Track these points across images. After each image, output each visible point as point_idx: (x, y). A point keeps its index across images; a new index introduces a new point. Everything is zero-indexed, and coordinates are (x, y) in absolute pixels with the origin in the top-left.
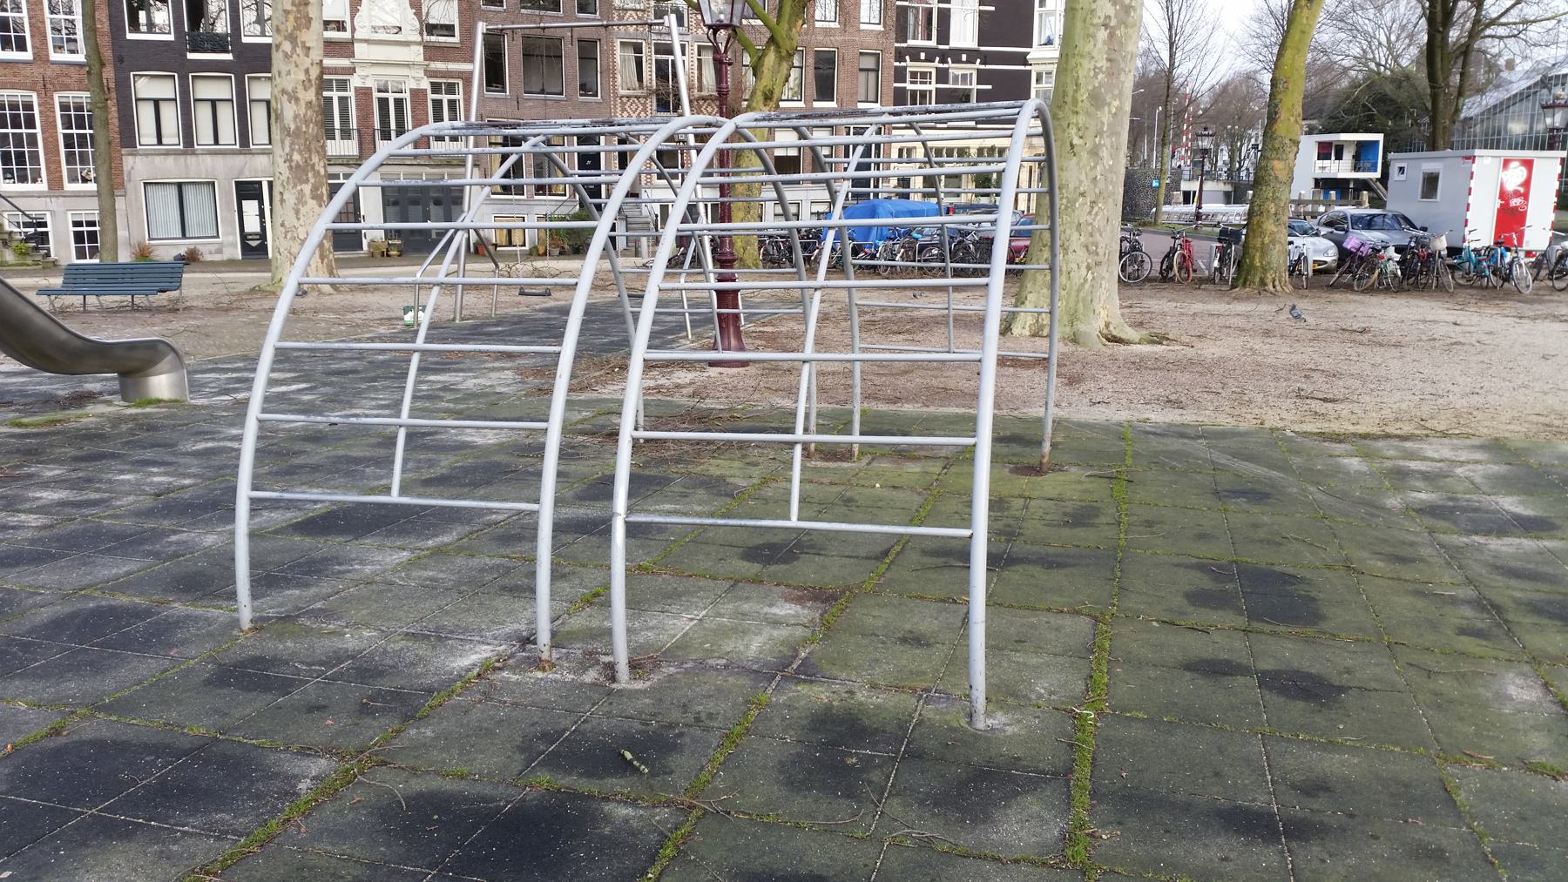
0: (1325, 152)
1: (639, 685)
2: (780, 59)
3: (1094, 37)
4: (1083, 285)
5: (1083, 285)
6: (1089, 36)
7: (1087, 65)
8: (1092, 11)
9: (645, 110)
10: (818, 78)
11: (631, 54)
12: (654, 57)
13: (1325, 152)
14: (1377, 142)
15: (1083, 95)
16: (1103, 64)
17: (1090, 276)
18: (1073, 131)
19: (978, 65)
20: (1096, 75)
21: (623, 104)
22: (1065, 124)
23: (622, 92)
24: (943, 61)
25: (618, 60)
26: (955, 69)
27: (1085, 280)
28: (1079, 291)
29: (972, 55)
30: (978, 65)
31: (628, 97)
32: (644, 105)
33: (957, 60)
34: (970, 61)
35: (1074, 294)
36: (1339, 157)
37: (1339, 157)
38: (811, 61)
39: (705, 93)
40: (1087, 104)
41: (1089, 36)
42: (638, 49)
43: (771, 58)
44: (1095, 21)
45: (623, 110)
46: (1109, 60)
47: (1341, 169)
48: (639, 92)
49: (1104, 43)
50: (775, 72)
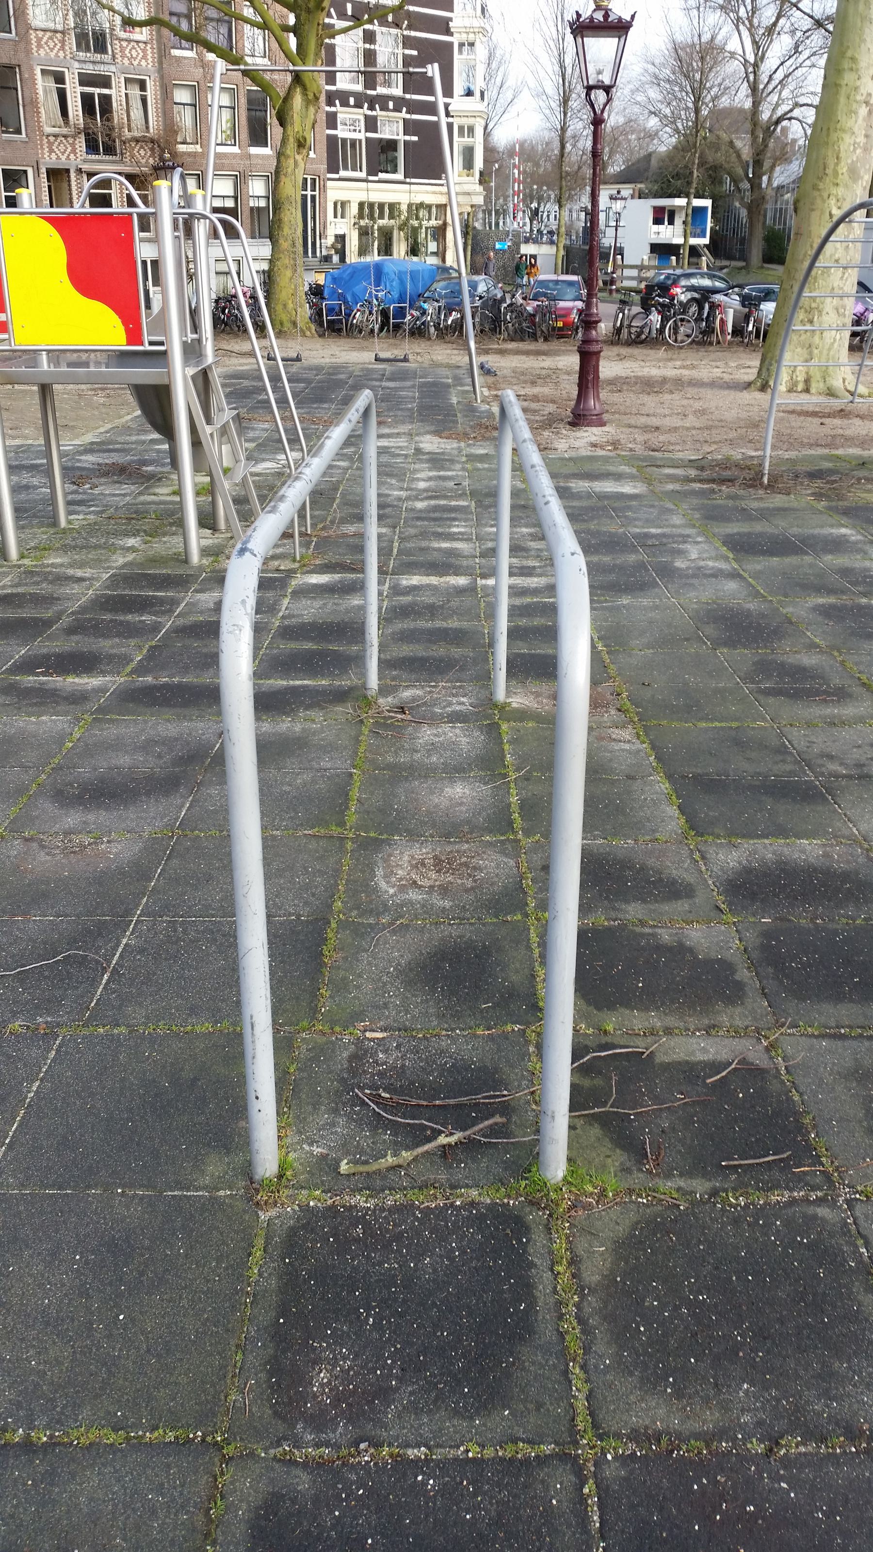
0: (660, 216)
1: (517, 701)
2: (307, 102)
3: (856, 113)
4: (832, 344)
5: (832, 344)
6: (851, 112)
7: (848, 139)
8: (856, 89)
9: (74, 151)
10: (251, 121)
11: (53, 85)
12: (79, 89)
13: (660, 216)
14: (706, 208)
15: (843, 169)
16: (861, 139)
17: (838, 337)
18: (832, 202)
19: (404, 114)
20: (855, 150)
21: (50, 144)
22: (825, 195)
23: (48, 130)
24: (372, 108)
25: (40, 91)
26: (344, 114)
27: (835, 340)
28: (829, 349)
29: (400, 104)
30: (404, 114)
31: (56, 136)
32: (73, 145)
33: (345, 104)
34: (397, 109)
35: (825, 352)
36: (671, 222)
37: (671, 222)
38: (243, 101)
39: (136, 134)
40: (846, 176)
41: (851, 112)
42: (59, 78)
43: (298, 100)
44: (859, 98)
45: (51, 151)
46: (866, 136)
47: (670, 234)
48: (65, 131)
49: (864, 119)
50: (304, 117)
